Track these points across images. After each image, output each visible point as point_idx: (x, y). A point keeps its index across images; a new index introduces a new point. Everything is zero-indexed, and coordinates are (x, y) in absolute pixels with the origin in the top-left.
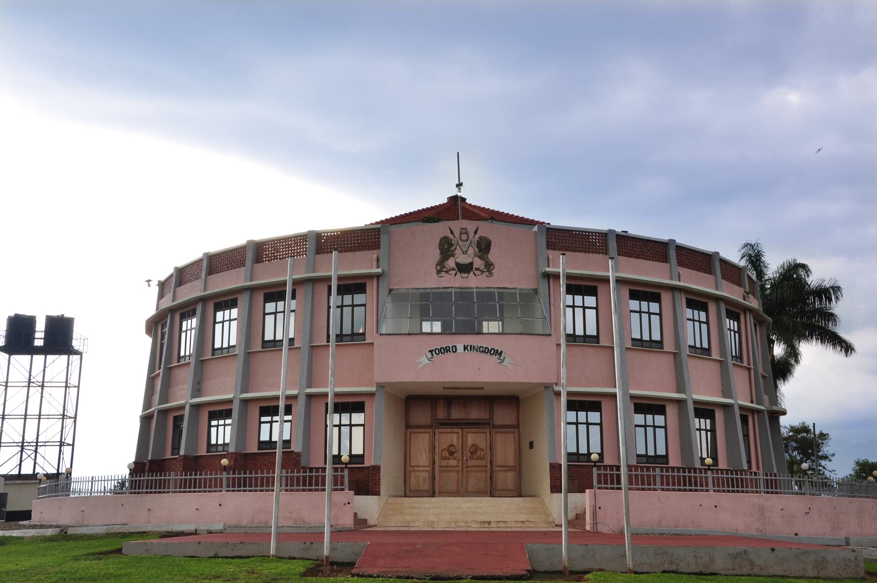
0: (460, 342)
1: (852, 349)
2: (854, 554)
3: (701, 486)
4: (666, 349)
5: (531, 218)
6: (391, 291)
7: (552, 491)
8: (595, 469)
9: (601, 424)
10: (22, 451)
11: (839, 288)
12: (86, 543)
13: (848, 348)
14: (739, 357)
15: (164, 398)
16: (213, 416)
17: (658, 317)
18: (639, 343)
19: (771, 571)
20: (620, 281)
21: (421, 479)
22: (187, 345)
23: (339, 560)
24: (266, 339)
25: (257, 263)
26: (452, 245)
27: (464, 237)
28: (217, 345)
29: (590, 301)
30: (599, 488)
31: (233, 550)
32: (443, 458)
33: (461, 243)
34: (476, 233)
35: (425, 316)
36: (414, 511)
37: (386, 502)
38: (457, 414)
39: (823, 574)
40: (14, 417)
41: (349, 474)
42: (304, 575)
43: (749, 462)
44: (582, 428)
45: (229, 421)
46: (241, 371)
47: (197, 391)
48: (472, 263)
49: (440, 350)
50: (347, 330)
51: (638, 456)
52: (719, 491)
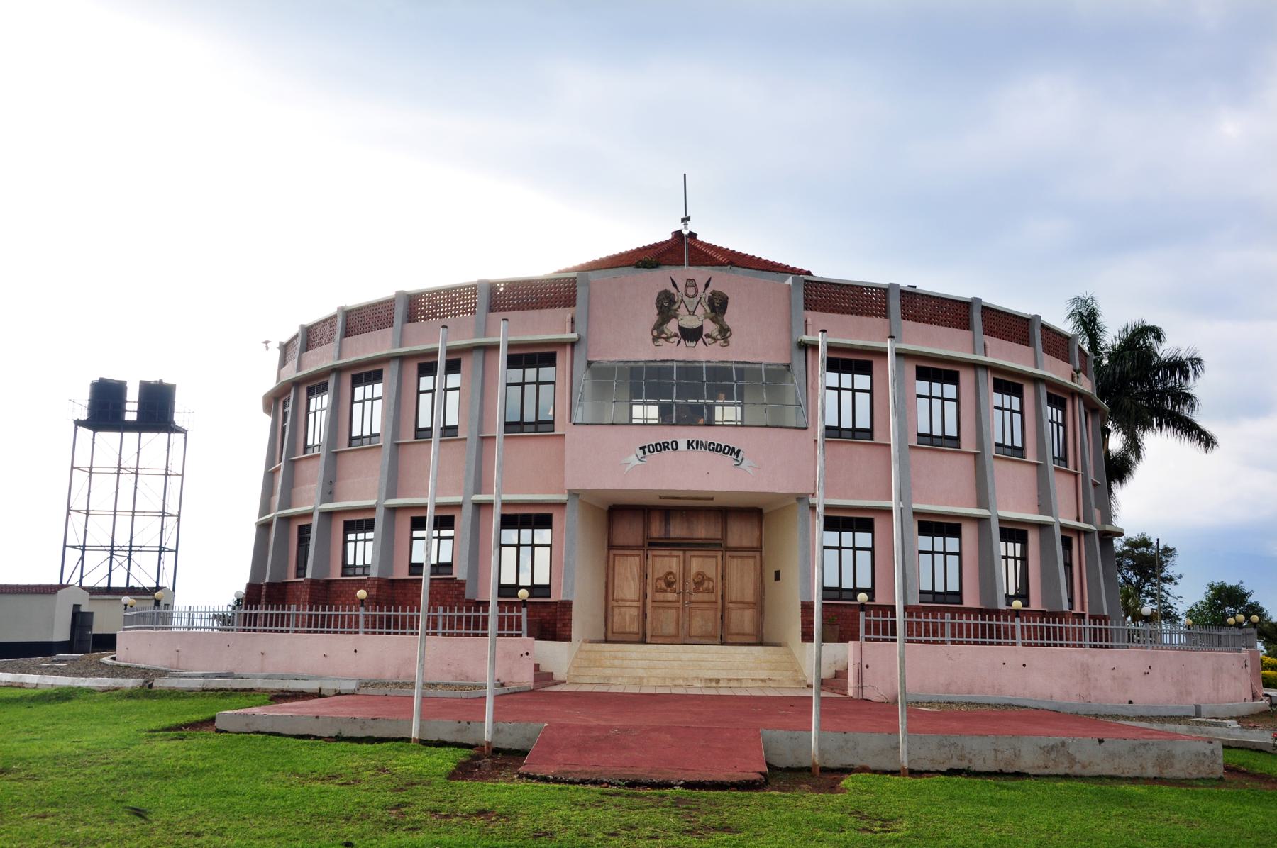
0: (683, 435)
1: (1214, 443)
2: (1211, 747)
3: (1006, 637)
4: (964, 448)
5: (785, 263)
6: (589, 364)
7: (804, 640)
8: (862, 614)
9: (872, 550)
10: (111, 558)
11: (1199, 360)
12: (175, 703)
13: (1207, 441)
14: (1064, 459)
15: (287, 502)
16: (350, 527)
17: (955, 404)
18: (928, 439)
19: (1097, 770)
20: (902, 355)
21: (627, 618)
22: (317, 430)
23: (505, 746)
24: (421, 426)
25: (409, 322)
26: (674, 302)
27: (691, 291)
28: (356, 433)
29: (862, 381)
30: (867, 640)
31: (362, 728)
32: (658, 590)
33: (686, 299)
34: (707, 285)
35: (635, 395)
36: (616, 662)
37: (580, 650)
38: (678, 530)
39: (1168, 773)
40: (101, 513)
41: (528, 616)
42: (452, 776)
43: (1071, 600)
44: (526, 551)
45: (370, 535)
46: (386, 468)
47: (329, 493)
48: (701, 328)
49: (665, 448)
50: (529, 416)
51: (921, 592)
52: (1029, 645)
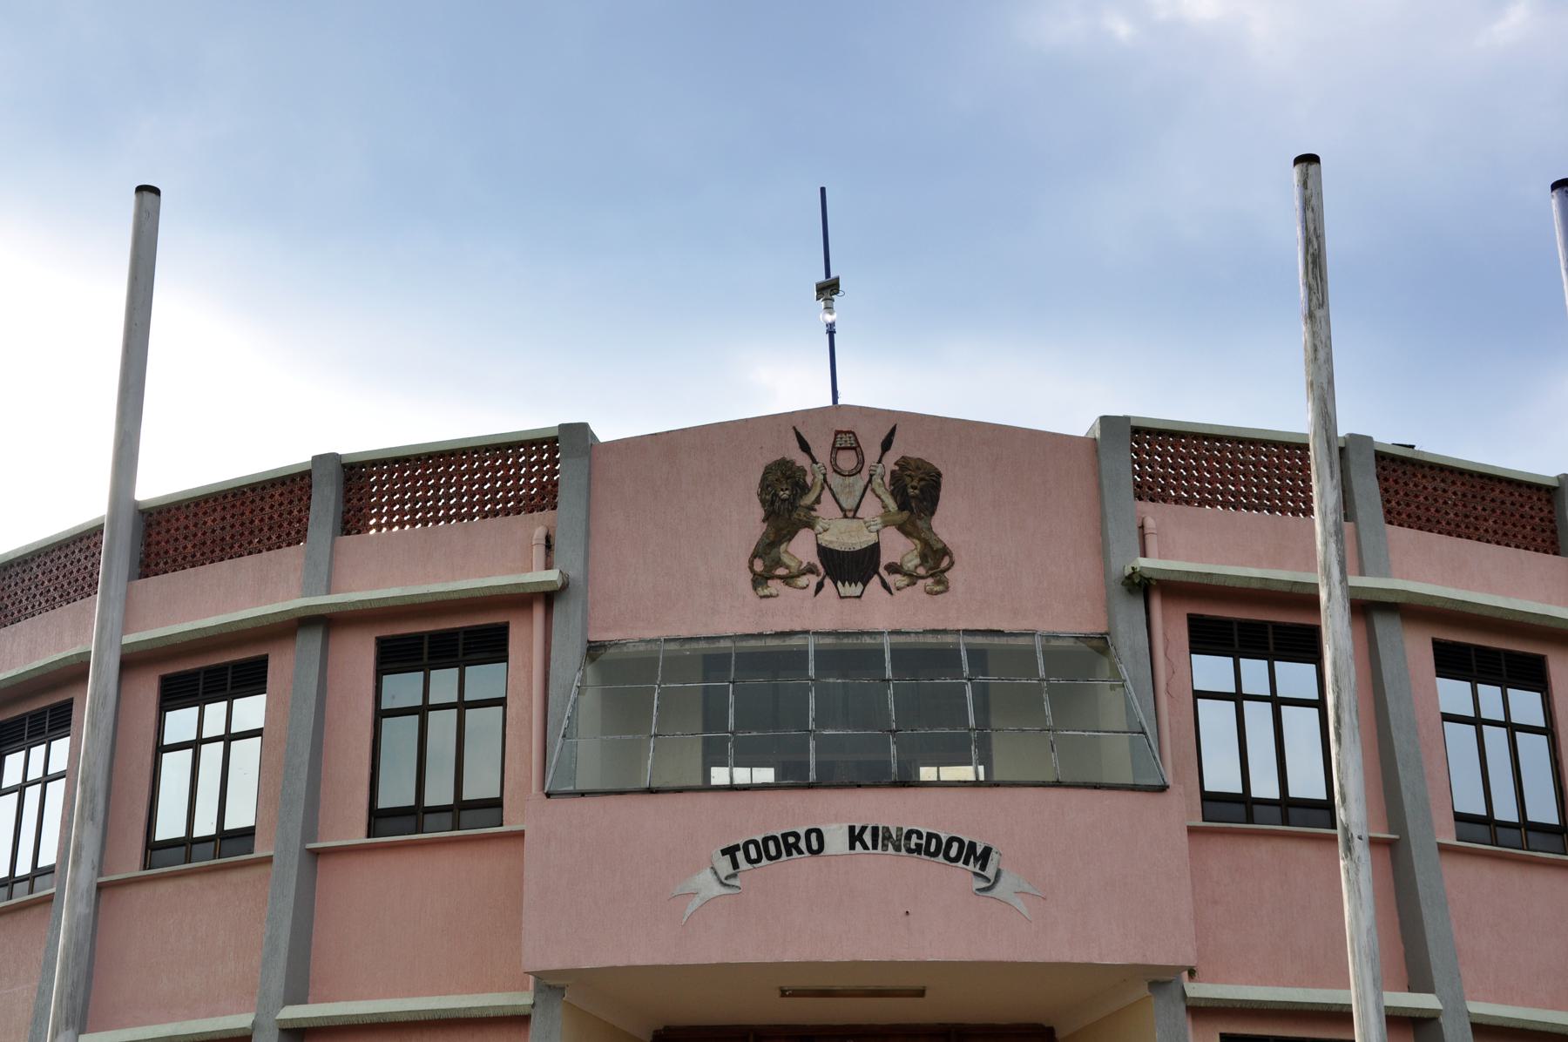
17: (1542, 740)
18: (1482, 830)
24: (161, 834)
27: (847, 460)
28: (169, 826)
33: (835, 480)
34: (887, 445)
48: (874, 550)
50: (439, 793)
